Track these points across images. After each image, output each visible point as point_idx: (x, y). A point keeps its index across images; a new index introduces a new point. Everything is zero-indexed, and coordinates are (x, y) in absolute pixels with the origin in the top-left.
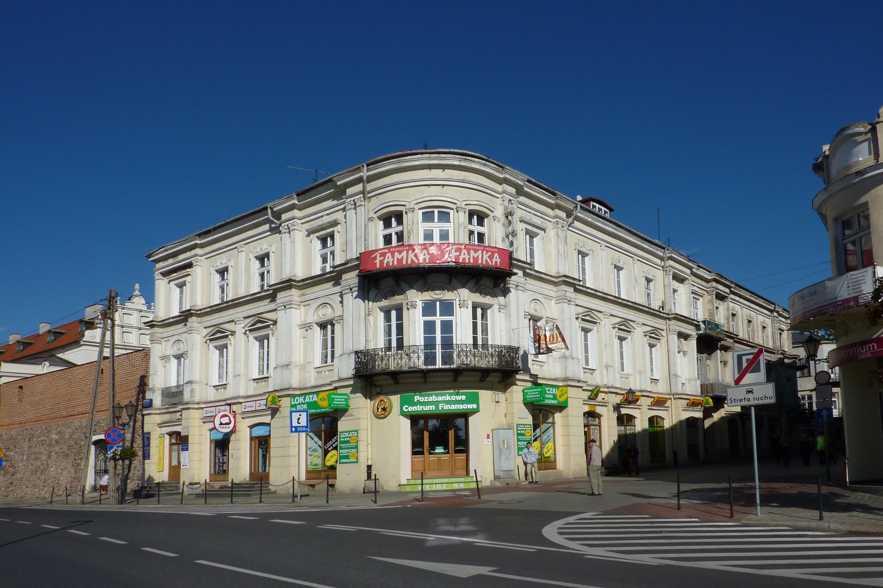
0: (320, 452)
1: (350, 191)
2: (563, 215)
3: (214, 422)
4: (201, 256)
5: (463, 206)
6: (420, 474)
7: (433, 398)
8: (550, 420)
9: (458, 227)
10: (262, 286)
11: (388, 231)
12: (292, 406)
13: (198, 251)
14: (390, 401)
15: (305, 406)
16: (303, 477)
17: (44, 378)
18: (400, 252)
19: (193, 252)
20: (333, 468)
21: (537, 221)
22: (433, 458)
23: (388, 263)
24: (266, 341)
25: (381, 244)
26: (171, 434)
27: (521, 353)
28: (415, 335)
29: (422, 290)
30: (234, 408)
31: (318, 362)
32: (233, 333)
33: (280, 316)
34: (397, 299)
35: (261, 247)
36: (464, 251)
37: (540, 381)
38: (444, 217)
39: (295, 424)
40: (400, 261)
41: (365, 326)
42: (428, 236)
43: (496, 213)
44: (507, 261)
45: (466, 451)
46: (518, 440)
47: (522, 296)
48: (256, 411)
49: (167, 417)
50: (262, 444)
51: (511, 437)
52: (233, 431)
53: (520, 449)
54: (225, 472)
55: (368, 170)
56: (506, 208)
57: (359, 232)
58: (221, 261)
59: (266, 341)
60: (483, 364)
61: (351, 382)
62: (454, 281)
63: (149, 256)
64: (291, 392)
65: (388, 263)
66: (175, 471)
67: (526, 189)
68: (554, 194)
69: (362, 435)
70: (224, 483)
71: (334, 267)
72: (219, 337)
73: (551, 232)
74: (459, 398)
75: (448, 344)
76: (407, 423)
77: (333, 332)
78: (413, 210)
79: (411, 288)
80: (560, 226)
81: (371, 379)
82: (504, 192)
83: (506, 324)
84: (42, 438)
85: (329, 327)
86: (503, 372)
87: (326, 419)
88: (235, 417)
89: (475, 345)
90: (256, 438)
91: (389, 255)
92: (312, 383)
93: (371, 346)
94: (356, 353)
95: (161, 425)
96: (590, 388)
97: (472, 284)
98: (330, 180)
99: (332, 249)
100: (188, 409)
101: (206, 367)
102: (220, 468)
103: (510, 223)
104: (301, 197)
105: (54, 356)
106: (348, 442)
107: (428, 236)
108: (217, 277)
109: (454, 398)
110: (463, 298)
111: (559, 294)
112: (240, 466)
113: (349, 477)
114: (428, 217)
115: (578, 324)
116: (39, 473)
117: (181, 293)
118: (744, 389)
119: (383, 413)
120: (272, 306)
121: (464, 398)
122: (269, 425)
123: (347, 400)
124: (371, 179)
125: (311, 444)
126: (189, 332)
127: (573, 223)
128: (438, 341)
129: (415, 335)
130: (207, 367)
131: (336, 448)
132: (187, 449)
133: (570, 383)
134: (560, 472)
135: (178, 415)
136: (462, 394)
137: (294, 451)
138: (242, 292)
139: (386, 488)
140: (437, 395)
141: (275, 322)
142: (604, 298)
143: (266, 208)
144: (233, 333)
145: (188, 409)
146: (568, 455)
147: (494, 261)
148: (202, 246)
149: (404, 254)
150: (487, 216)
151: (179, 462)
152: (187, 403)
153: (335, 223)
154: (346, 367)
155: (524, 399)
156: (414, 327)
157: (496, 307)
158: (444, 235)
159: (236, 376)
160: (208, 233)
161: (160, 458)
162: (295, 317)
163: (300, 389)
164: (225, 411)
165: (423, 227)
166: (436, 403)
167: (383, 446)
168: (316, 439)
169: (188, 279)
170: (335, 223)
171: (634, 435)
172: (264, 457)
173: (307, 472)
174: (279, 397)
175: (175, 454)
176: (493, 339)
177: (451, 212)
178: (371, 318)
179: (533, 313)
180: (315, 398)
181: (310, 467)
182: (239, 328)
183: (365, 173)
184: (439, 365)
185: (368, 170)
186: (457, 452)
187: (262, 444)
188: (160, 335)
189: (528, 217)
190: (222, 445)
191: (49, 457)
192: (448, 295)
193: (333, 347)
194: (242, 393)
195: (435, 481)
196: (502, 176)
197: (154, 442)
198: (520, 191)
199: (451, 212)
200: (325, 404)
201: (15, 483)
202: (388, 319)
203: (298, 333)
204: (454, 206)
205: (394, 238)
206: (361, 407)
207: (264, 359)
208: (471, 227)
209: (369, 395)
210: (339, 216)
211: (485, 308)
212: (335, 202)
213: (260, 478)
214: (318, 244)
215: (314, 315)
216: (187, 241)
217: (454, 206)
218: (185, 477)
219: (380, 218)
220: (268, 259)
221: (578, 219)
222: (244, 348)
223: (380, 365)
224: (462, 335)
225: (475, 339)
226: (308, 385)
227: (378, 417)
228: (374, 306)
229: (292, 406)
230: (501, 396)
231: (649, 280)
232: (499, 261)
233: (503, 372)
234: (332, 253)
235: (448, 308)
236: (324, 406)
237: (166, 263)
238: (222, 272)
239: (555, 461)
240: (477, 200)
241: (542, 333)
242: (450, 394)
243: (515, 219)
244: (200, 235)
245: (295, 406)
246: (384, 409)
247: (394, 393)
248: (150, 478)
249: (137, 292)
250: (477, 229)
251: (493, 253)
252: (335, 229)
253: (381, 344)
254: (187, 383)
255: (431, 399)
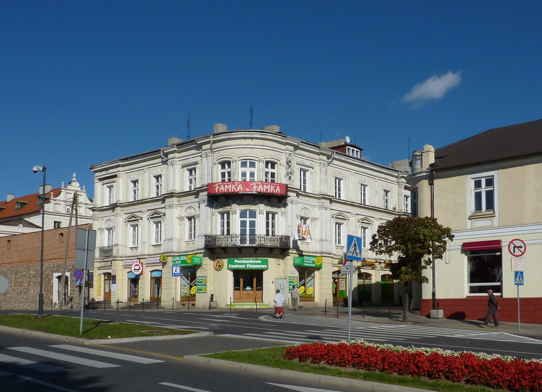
0: (188, 287)
1: (204, 147)
2: (325, 158)
3: (131, 268)
4: (122, 171)
5: (263, 159)
6: (236, 299)
7: (244, 261)
8: (313, 275)
9: (259, 172)
10: (158, 193)
11: (223, 171)
12: (173, 261)
13: (121, 169)
14: (222, 262)
15: (180, 262)
16: (179, 299)
17: (25, 236)
18: (228, 185)
19: (118, 169)
20: (194, 295)
21: (308, 163)
22: (245, 292)
23: (222, 190)
24: (159, 224)
25: (220, 179)
26: (105, 274)
27: (291, 239)
28: (236, 229)
29: (239, 204)
30: (142, 261)
31: (187, 239)
32: (141, 218)
33: (167, 211)
34: (227, 208)
35: (158, 170)
36: (261, 185)
37: (304, 254)
38: (252, 165)
39: (174, 272)
40: (228, 189)
41: (211, 222)
42: (244, 174)
43: (281, 162)
44: (284, 190)
45: (262, 290)
46: (290, 285)
47: (295, 207)
48: (154, 263)
49: (103, 264)
50: (157, 281)
51: (286, 285)
52: (141, 274)
53: (290, 290)
54: (136, 297)
55: (213, 138)
56: (287, 159)
57: (209, 172)
58: (134, 176)
59: (159, 224)
60: (269, 244)
61: (203, 251)
62: (256, 200)
63: (91, 169)
64: (173, 254)
65: (222, 190)
66: (108, 295)
67: (300, 146)
68: (319, 147)
69: (209, 279)
70: (136, 303)
71: (196, 189)
72: (133, 220)
73: (317, 168)
74: (257, 262)
75: (252, 233)
76: (231, 274)
77: (195, 223)
78: (236, 161)
79: (234, 203)
80: (322, 165)
81: (214, 250)
82: (286, 150)
83: (285, 223)
84: (24, 273)
85: (193, 219)
86: (281, 250)
87: (191, 269)
88: (142, 266)
89: (268, 234)
90: (154, 278)
91: (222, 186)
92: (184, 250)
93: (214, 233)
94: (206, 236)
95: (99, 269)
96: (340, 258)
97: (266, 201)
98: (194, 140)
99: (195, 176)
100: (116, 260)
101: (126, 237)
102: (133, 294)
103: (290, 166)
104: (179, 147)
105: (22, 219)
106: (201, 282)
107: (244, 174)
108: (132, 185)
109: (255, 262)
110: (261, 209)
111: (320, 204)
112: (145, 292)
113: (202, 301)
114: (244, 164)
115: (334, 221)
116: (22, 294)
117: (110, 191)
118: (346, 267)
119: (219, 268)
120: (163, 205)
121: (260, 262)
122: (161, 271)
123: (201, 260)
124: (214, 142)
125: (183, 282)
126: (116, 215)
127: (332, 161)
128: (248, 232)
129: (236, 229)
130: (126, 237)
131: (195, 285)
132: (115, 283)
133: (323, 255)
134: (317, 303)
135: (109, 263)
136: (259, 260)
137: (174, 286)
138: (146, 196)
139: (220, 306)
140: (246, 260)
141: (164, 215)
142: (352, 205)
143: (160, 150)
144: (141, 218)
145: (116, 260)
146: (321, 295)
147: (277, 190)
148: (123, 166)
149: (230, 186)
150: (277, 163)
151: (110, 290)
152: (115, 257)
153: (196, 163)
154: (200, 243)
155: (294, 263)
156: (235, 224)
157: (280, 213)
158: (252, 174)
159: (143, 243)
160: (126, 159)
161: (99, 288)
162: (175, 212)
163: (177, 253)
164: (137, 262)
165: (241, 170)
166: (245, 264)
167: (219, 284)
168: (186, 280)
169: (114, 184)
170: (196, 163)
171: (370, 285)
172: (158, 289)
173: (181, 297)
174: (167, 256)
175: (107, 285)
176: (278, 232)
177: (256, 162)
178: (214, 217)
179: (303, 215)
180: (185, 258)
181: (183, 295)
182: (145, 216)
183: (211, 139)
184: (248, 244)
185: (213, 138)
186: (257, 290)
187: (157, 281)
188: (98, 216)
189: (301, 161)
190: (135, 281)
191: (29, 284)
192: (253, 207)
193: (195, 231)
194: (146, 253)
195: (245, 304)
196: (285, 141)
197: (95, 278)
198: (296, 148)
199: (256, 162)
200: (190, 261)
201: (7, 300)
202: (223, 218)
203: (176, 222)
204: (257, 159)
205: (227, 175)
206: (208, 264)
207: (158, 233)
208: (267, 170)
209: (212, 258)
210: (198, 159)
211: (274, 214)
212: (197, 151)
213: (156, 300)
214: (188, 173)
215: (185, 214)
216: (114, 162)
217: (257, 159)
218: (113, 300)
219: (219, 163)
220: (161, 178)
221: (335, 159)
222: (147, 227)
223: (218, 244)
224: (261, 230)
225: (267, 231)
226: (182, 251)
227: (216, 270)
228: (216, 211)
229: (173, 261)
230: (281, 261)
231: (387, 192)
232: (279, 190)
233: (281, 250)
234: (195, 179)
235: (253, 214)
236: (189, 263)
237: (101, 174)
238: (135, 182)
239: (314, 297)
240: (270, 155)
241: (301, 229)
242: (253, 260)
243: (294, 164)
244: (122, 160)
245: (175, 261)
246: (220, 266)
247: (225, 258)
248: (93, 299)
249: (74, 179)
250: (270, 170)
251: (276, 186)
252: (196, 166)
253: (219, 233)
254: (115, 245)
255: (243, 262)
